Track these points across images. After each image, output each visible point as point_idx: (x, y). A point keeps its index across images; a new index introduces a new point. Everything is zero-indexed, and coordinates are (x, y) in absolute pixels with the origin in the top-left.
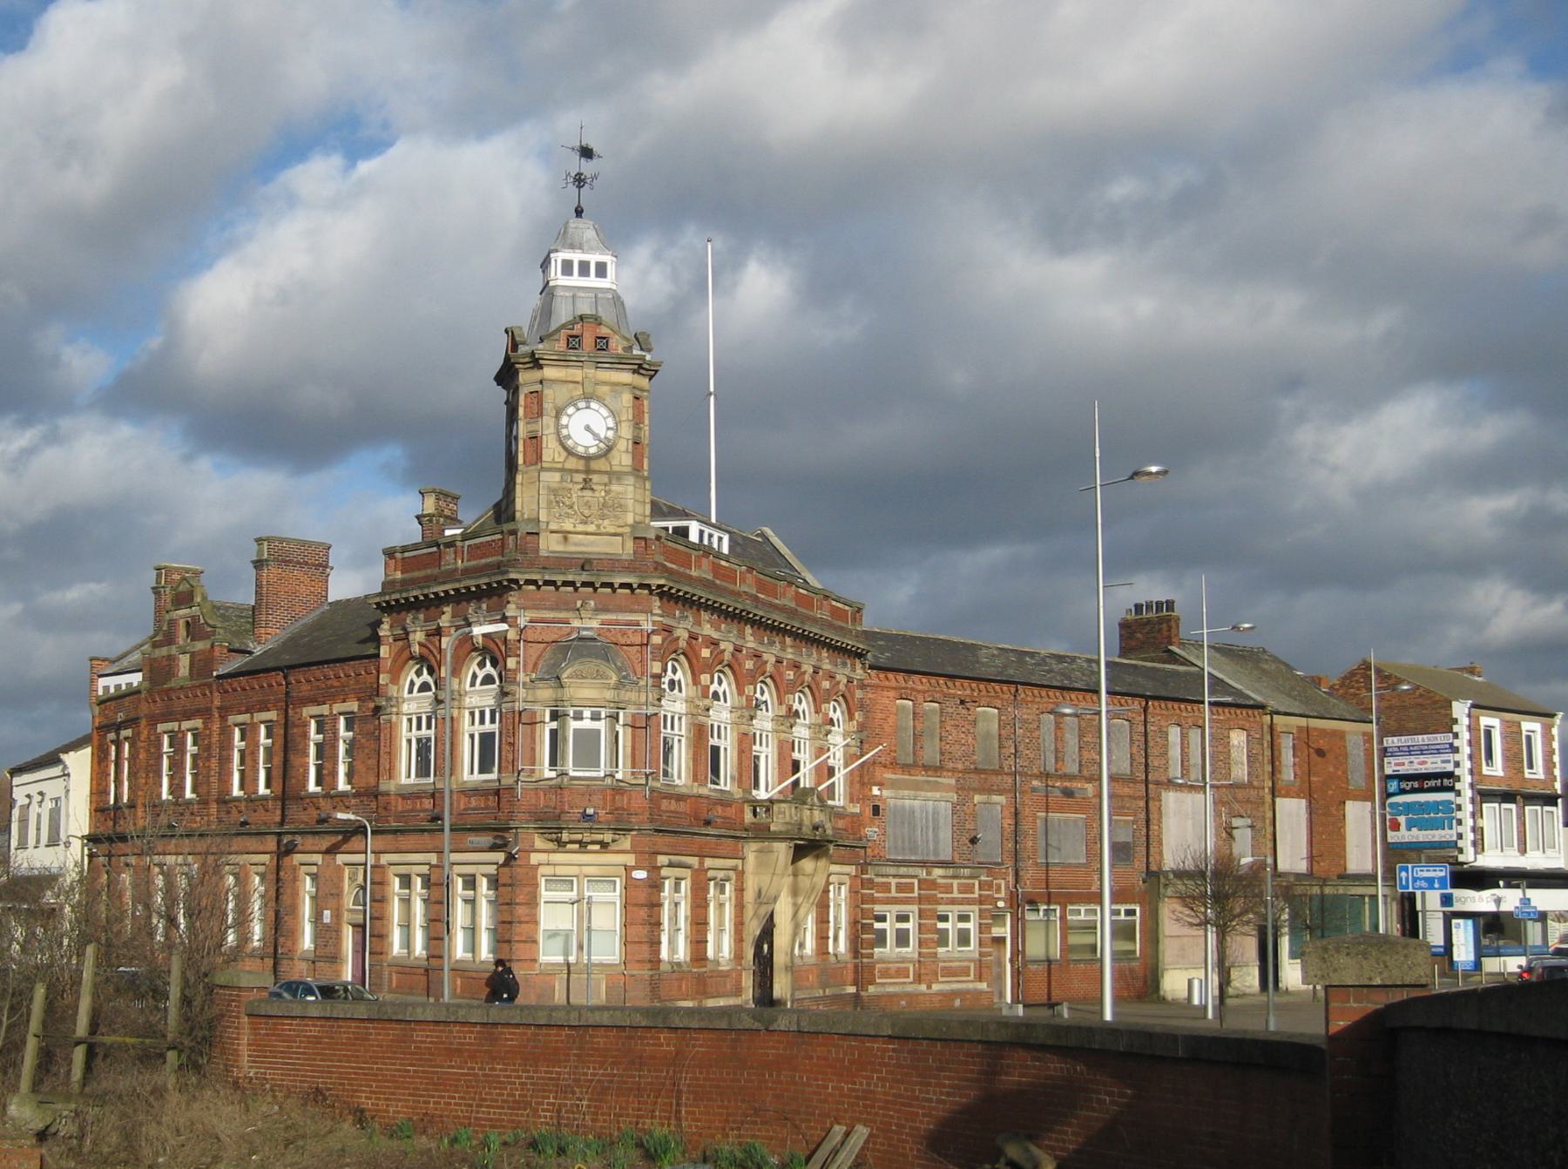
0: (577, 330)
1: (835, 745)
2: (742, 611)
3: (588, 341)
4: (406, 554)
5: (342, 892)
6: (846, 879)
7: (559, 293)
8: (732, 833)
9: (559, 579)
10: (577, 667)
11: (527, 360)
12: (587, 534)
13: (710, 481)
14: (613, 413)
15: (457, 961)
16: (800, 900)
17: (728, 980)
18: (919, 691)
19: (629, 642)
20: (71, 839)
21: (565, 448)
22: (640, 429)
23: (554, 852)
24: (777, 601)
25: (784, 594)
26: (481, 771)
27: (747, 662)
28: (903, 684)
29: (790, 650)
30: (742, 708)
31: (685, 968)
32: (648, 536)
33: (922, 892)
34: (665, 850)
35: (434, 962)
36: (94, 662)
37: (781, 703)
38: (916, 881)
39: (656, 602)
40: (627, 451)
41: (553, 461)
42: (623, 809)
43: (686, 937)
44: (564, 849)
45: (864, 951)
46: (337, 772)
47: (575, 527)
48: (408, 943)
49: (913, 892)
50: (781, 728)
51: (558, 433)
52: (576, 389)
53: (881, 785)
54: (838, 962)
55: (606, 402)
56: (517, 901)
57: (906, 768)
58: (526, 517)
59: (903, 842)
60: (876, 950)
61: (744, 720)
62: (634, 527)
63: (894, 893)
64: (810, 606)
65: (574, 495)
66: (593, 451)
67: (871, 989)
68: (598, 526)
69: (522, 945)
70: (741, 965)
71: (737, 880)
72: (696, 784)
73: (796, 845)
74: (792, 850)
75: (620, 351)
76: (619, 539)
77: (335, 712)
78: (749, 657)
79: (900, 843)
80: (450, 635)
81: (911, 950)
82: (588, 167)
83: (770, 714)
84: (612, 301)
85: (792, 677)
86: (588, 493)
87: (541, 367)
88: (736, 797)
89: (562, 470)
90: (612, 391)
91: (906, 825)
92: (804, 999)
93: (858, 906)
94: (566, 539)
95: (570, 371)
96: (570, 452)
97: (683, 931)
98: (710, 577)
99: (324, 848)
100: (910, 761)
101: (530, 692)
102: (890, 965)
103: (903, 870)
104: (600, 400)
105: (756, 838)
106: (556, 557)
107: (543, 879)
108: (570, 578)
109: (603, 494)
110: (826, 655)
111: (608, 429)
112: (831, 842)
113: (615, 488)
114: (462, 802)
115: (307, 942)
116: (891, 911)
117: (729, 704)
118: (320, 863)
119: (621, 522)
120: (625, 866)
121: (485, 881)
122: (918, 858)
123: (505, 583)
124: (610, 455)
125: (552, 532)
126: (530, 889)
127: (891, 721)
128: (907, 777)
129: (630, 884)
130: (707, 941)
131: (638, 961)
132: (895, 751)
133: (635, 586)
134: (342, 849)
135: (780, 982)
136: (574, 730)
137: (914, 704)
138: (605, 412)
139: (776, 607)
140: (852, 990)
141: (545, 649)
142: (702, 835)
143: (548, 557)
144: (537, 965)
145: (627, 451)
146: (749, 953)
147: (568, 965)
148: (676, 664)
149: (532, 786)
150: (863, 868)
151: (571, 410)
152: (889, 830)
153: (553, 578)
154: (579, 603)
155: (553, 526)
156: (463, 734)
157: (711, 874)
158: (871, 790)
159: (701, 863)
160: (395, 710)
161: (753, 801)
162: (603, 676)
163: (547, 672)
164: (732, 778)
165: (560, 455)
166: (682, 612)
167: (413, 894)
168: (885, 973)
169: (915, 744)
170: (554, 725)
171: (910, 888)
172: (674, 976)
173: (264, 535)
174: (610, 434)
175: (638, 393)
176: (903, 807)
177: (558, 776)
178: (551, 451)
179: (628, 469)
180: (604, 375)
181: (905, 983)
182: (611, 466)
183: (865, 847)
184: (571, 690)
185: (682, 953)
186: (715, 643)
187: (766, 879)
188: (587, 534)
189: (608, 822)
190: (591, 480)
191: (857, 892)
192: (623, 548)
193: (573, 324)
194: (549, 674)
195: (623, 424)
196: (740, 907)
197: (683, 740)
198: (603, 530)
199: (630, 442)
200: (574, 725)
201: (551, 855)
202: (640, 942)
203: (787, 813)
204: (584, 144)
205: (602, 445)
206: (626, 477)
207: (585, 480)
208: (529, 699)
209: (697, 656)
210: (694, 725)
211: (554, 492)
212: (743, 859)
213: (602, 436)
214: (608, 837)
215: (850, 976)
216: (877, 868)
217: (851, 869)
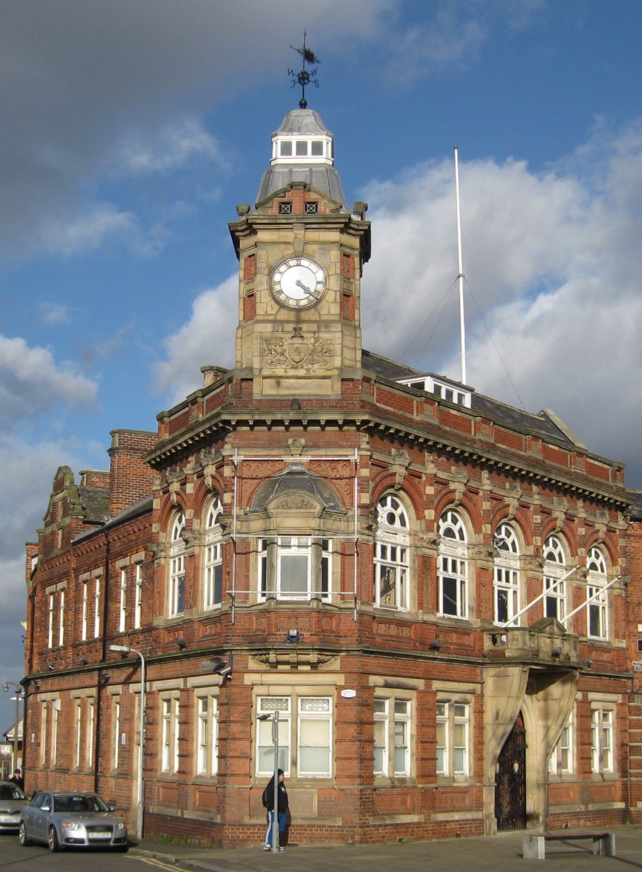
3: (298, 207)
5: (133, 716)
7: (277, 170)
8: (466, 658)
9: (269, 418)
10: (282, 499)
12: (298, 378)
15: (197, 777)
16: (550, 722)
17: (467, 795)
20: (9, 685)
21: (278, 302)
23: (266, 672)
24: (522, 453)
25: (529, 447)
27: (484, 503)
29: (536, 497)
31: (409, 784)
32: (355, 377)
34: (381, 671)
36: (28, 546)
39: (365, 438)
40: (335, 302)
41: (266, 314)
43: (412, 755)
44: (275, 670)
45: (632, 771)
47: (286, 372)
48: (208, 764)
50: (529, 566)
51: (271, 289)
52: (287, 249)
54: (604, 780)
55: (315, 259)
56: (232, 719)
58: (244, 366)
61: (482, 556)
66: (303, 303)
68: (308, 370)
69: (235, 761)
70: (482, 782)
71: (476, 703)
72: (421, 611)
74: (527, 675)
76: (328, 381)
77: (132, 563)
78: (484, 499)
80: (193, 482)
82: (309, 67)
83: (518, 553)
84: (325, 173)
85: (539, 521)
86: (298, 341)
87: (254, 232)
88: (474, 626)
89: (274, 321)
90: (321, 249)
92: (560, 814)
93: (626, 731)
94: (278, 383)
96: (282, 305)
97: (409, 749)
101: (244, 524)
104: (310, 258)
107: (259, 699)
109: (312, 341)
111: (318, 283)
113: (324, 335)
118: (121, 693)
119: (329, 365)
121: (215, 701)
124: (319, 306)
125: (265, 378)
126: (244, 708)
129: (341, 704)
130: (218, 757)
131: (348, 777)
133: (340, 422)
134: (133, 680)
135: (532, 798)
136: (282, 557)
139: (521, 458)
140: (620, 805)
141: (258, 484)
143: (261, 400)
144: (252, 780)
146: (491, 770)
149: (245, 611)
151: (283, 268)
153: (263, 418)
155: (266, 372)
156: (203, 569)
157: (440, 696)
160: (163, 554)
163: (259, 505)
164: (471, 609)
165: (273, 309)
166: (398, 450)
170: (265, 554)
172: (395, 791)
173: (115, 428)
174: (320, 287)
175: (348, 251)
177: (267, 600)
179: (337, 318)
180: (312, 235)
182: (320, 315)
183: (632, 678)
184: (278, 519)
185: (408, 769)
188: (298, 378)
189: (312, 643)
190: (300, 329)
193: (285, 192)
194: (259, 507)
195: (331, 278)
196: (479, 728)
197: (408, 570)
198: (312, 374)
199: (338, 294)
200: (281, 552)
201: (264, 675)
202: (350, 759)
203: (520, 639)
204: (307, 48)
205: (311, 298)
207: (295, 329)
209: (420, 493)
210: (418, 556)
211: (267, 341)
212: (482, 683)
213: (312, 290)
214: (313, 657)
215: (619, 794)
217: (619, 698)
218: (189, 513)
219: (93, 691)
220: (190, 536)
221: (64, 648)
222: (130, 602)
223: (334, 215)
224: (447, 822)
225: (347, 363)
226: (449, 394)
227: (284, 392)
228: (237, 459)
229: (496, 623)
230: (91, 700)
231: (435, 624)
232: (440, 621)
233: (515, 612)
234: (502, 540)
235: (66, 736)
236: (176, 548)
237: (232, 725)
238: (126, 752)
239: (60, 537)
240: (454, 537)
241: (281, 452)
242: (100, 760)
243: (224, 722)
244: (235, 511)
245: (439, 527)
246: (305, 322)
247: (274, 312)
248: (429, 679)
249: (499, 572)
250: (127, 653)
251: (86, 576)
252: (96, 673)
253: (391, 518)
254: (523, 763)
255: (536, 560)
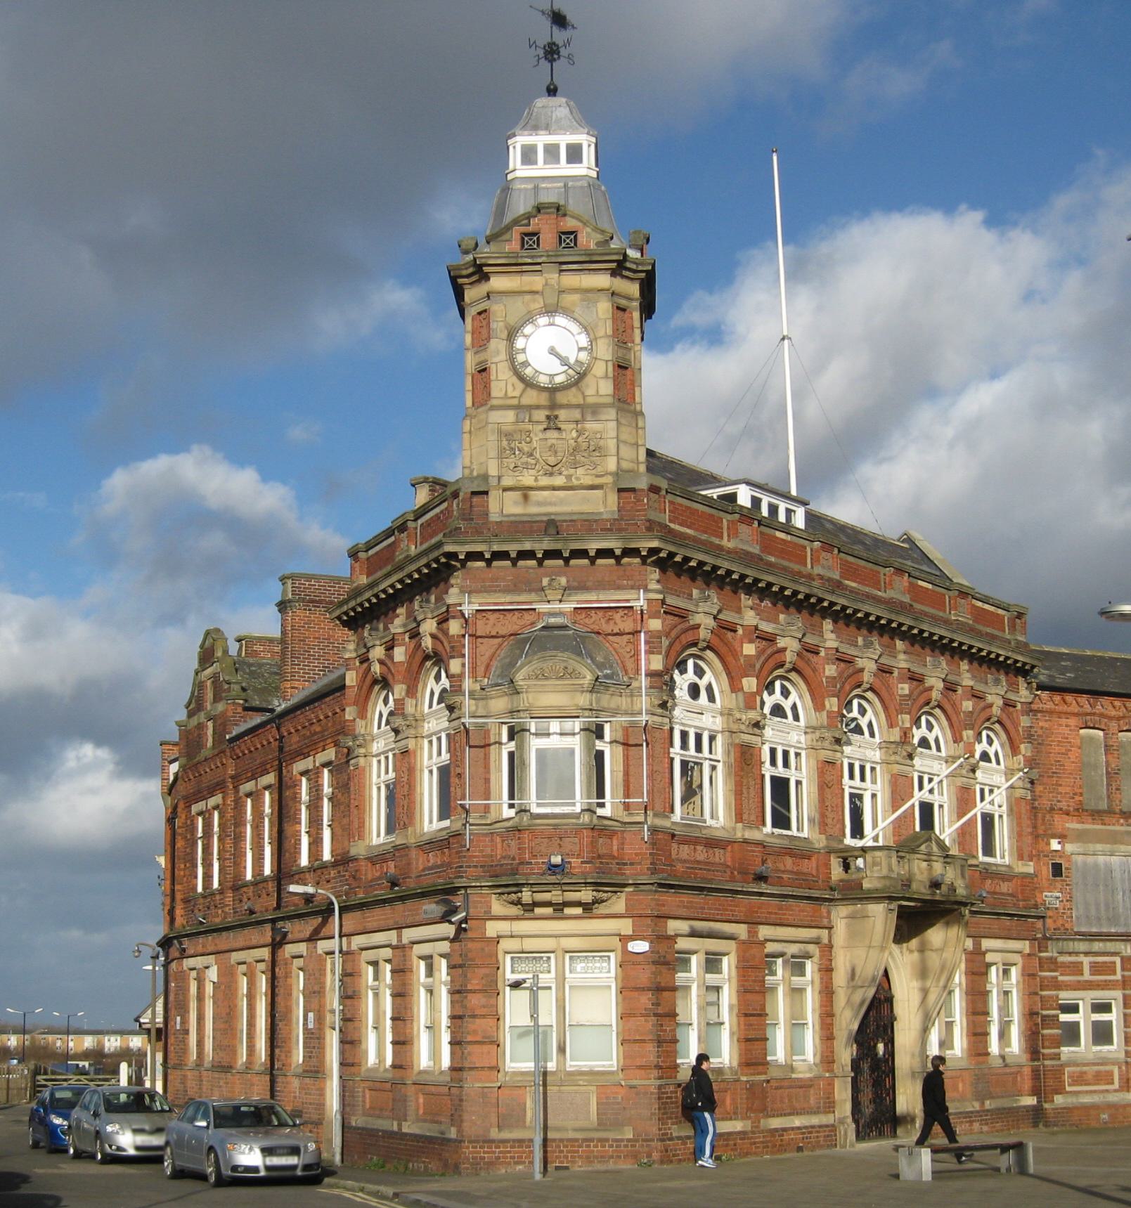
0: (535, 224)
1: (999, 788)
2: (808, 597)
3: (548, 239)
4: (371, 552)
6: (1017, 958)
7: (517, 186)
8: (807, 893)
9: (513, 548)
11: (471, 270)
12: (554, 488)
13: (788, 448)
14: (586, 328)
15: (421, 1072)
16: (928, 984)
18: (1111, 718)
19: (616, 630)
20: (141, 948)
21: (522, 378)
22: (630, 349)
23: (517, 918)
24: (880, 593)
26: (441, 818)
28: (1088, 708)
29: (902, 656)
30: (822, 727)
31: (728, 1076)
33: (1126, 973)
34: (683, 912)
35: (399, 1073)
36: (164, 747)
37: (891, 726)
38: (1118, 960)
39: (655, 574)
40: (606, 377)
41: (506, 396)
42: (614, 858)
43: (732, 1034)
45: (1046, 1051)
46: (322, 839)
47: (536, 480)
48: (435, 1054)
49: (1114, 973)
50: (893, 758)
51: (512, 360)
52: (534, 301)
53: (1062, 837)
54: (1006, 1066)
55: (576, 315)
56: (469, 987)
57: (1096, 815)
59: (1098, 909)
60: (1062, 1048)
61: (826, 744)
62: (617, 475)
63: (1087, 976)
64: (939, 602)
65: (535, 439)
66: (559, 379)
67: (1059, 1100)
68: (569, 477)
71: (821, 958)
72: (740, 825)
73: (900, 907)
75: (592, 246)
79: (1093, 912)
81: (1115, 1048)
82: (560, 36)
85: (907, 692)
86: (552, 434)
87: (485, 277)
88: (817, 846)
89: (518, 407)
91: (1101, 888)
93: (1036, 994)
94: (526, 497)
95: (526, 278)
96: (528, 383)
97: (727, 1025)
98: (755, 549)
99: (307, 934)
100: (1104, 805)
101: (481, 703)
102: (1085, 1069)
103: (1097, 946)
104: (568, 313)
105: (845, 899)
106: (512, 522)
108: (527, 546)
109: (574, 434)
110: (966, 667)
111: (580, 349)
112: (965, 904)
113: (591, 426)
114: (421, 861)
115: (299, 1055)
116: (1086, 1000)
117: (802, 723)
119: (600, 470)
120: (620, 935)
122: (1121, 930)
123: (443, 560)
124: (583, 384)
125: (505, 490)
127: (1072, 756)
128: (1103, 827)
131: (640, 1067)
132: (1081, 794)
133: (618, 552)
134: (322, 935)
137: (1106, 735)
138: (575, 328)
139: (878, 600)
140: (1030, 1101)
141: (500, 645)
142: (761, 894)
143: (501, 522)
145: (606, 377)
146: (845, 1054)
147: (545, 1074)
148: (700, 663)
149: (485, 829)
150: (1041, 943)
152: (1077, 895)
153: (504, 548)
154: (545, 581)
155: (507, 482)
156: (422, 771)
157: (771, 948)
158: (1048, 844)
159: (752, 933)
160: (362, 751)
161: (841, 851)
162: (573, 674)
163: (501, 676)
164: (811, 820)
166: (702, 591)
167: (382, 985)
168: (1079, 1079)
169: (1109, 785)
170: (512, 746)
171: (1111, 969)
173: (287, 572)
174: (584, 356)
175: (623, 302)
176: (1096, 865)
177: (517, 813)
178: (503, 383)
180: (571, 280)
181: (1107, 1091)
182: (584, 397)
184: (530, 696)
186: (769, 639)
187: (861, 953)
188: (554, 488)
190: (556, 417)
191: (1033, 975)
192: (604, 504)
193: (529, 218)
195: (600, 342)
196: (827, 993)
197: (720, 766)
198: (575, 482)
199: (610, 364)
200: (535, 744)
204: (556, 8)
205: (571, 372)
206: (605, 410)
207: (548, 417)
208: (481, 712)
209: (735, 654)
211: (509, 436)
212: (830, 928)
213: (572, 361)
214: (586, 895)
215: (1027, 1085)
216: (1060, 943)
217: (1025, 946)
218: (399, 690)
219: (265, 953)
220: (400, 724)
221: (221, 891)
222: (315, 822)
223: (601, 250)
224: (784, 1130)
225: (625, 465)
226: (773, 509)
227: (533, 510)
228: (467, 609)
229: (849, 841)
230: (262, 966)
231: (760, 844)
232: (768, 840)
233: (875, 825)
234: (854, 719)
235: (227, 1018)
236: (382, 743)
237: (470, 996)
238: (315, 1040)
239: (210, 732)
240: (785, 717)
241: (533, 597)
242: (277, 1051)
243: (459, 992)
244: (467, 684)
245: (763, 703)
246: (562, 406)
247: (517, 394)
248: (753, 923)
249: (851, 766)
250: (313, 896)
251: (248, 786)
252: (268, 927)
253: (694, 691)
254: (890, 1042)
255: (904, 748)
